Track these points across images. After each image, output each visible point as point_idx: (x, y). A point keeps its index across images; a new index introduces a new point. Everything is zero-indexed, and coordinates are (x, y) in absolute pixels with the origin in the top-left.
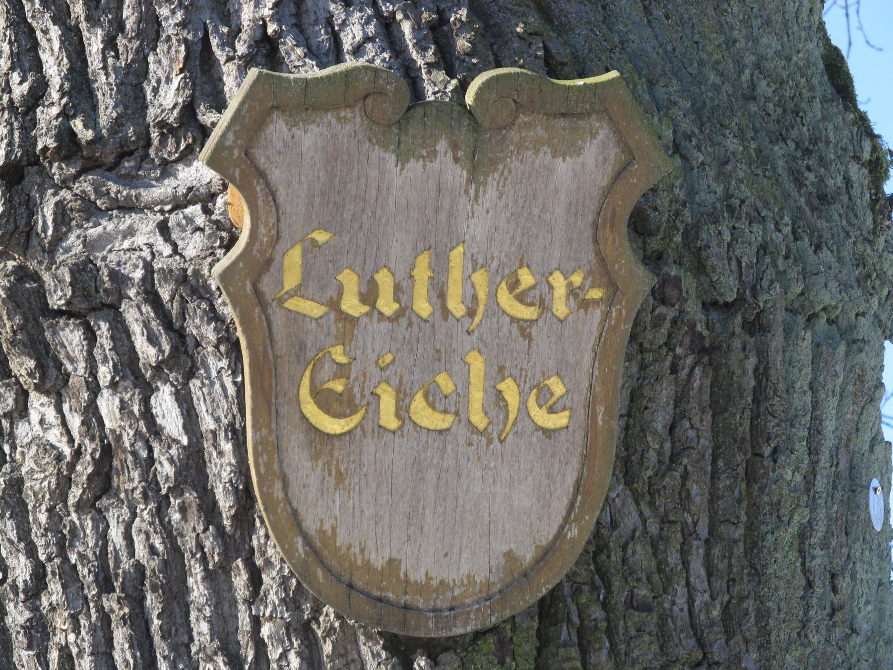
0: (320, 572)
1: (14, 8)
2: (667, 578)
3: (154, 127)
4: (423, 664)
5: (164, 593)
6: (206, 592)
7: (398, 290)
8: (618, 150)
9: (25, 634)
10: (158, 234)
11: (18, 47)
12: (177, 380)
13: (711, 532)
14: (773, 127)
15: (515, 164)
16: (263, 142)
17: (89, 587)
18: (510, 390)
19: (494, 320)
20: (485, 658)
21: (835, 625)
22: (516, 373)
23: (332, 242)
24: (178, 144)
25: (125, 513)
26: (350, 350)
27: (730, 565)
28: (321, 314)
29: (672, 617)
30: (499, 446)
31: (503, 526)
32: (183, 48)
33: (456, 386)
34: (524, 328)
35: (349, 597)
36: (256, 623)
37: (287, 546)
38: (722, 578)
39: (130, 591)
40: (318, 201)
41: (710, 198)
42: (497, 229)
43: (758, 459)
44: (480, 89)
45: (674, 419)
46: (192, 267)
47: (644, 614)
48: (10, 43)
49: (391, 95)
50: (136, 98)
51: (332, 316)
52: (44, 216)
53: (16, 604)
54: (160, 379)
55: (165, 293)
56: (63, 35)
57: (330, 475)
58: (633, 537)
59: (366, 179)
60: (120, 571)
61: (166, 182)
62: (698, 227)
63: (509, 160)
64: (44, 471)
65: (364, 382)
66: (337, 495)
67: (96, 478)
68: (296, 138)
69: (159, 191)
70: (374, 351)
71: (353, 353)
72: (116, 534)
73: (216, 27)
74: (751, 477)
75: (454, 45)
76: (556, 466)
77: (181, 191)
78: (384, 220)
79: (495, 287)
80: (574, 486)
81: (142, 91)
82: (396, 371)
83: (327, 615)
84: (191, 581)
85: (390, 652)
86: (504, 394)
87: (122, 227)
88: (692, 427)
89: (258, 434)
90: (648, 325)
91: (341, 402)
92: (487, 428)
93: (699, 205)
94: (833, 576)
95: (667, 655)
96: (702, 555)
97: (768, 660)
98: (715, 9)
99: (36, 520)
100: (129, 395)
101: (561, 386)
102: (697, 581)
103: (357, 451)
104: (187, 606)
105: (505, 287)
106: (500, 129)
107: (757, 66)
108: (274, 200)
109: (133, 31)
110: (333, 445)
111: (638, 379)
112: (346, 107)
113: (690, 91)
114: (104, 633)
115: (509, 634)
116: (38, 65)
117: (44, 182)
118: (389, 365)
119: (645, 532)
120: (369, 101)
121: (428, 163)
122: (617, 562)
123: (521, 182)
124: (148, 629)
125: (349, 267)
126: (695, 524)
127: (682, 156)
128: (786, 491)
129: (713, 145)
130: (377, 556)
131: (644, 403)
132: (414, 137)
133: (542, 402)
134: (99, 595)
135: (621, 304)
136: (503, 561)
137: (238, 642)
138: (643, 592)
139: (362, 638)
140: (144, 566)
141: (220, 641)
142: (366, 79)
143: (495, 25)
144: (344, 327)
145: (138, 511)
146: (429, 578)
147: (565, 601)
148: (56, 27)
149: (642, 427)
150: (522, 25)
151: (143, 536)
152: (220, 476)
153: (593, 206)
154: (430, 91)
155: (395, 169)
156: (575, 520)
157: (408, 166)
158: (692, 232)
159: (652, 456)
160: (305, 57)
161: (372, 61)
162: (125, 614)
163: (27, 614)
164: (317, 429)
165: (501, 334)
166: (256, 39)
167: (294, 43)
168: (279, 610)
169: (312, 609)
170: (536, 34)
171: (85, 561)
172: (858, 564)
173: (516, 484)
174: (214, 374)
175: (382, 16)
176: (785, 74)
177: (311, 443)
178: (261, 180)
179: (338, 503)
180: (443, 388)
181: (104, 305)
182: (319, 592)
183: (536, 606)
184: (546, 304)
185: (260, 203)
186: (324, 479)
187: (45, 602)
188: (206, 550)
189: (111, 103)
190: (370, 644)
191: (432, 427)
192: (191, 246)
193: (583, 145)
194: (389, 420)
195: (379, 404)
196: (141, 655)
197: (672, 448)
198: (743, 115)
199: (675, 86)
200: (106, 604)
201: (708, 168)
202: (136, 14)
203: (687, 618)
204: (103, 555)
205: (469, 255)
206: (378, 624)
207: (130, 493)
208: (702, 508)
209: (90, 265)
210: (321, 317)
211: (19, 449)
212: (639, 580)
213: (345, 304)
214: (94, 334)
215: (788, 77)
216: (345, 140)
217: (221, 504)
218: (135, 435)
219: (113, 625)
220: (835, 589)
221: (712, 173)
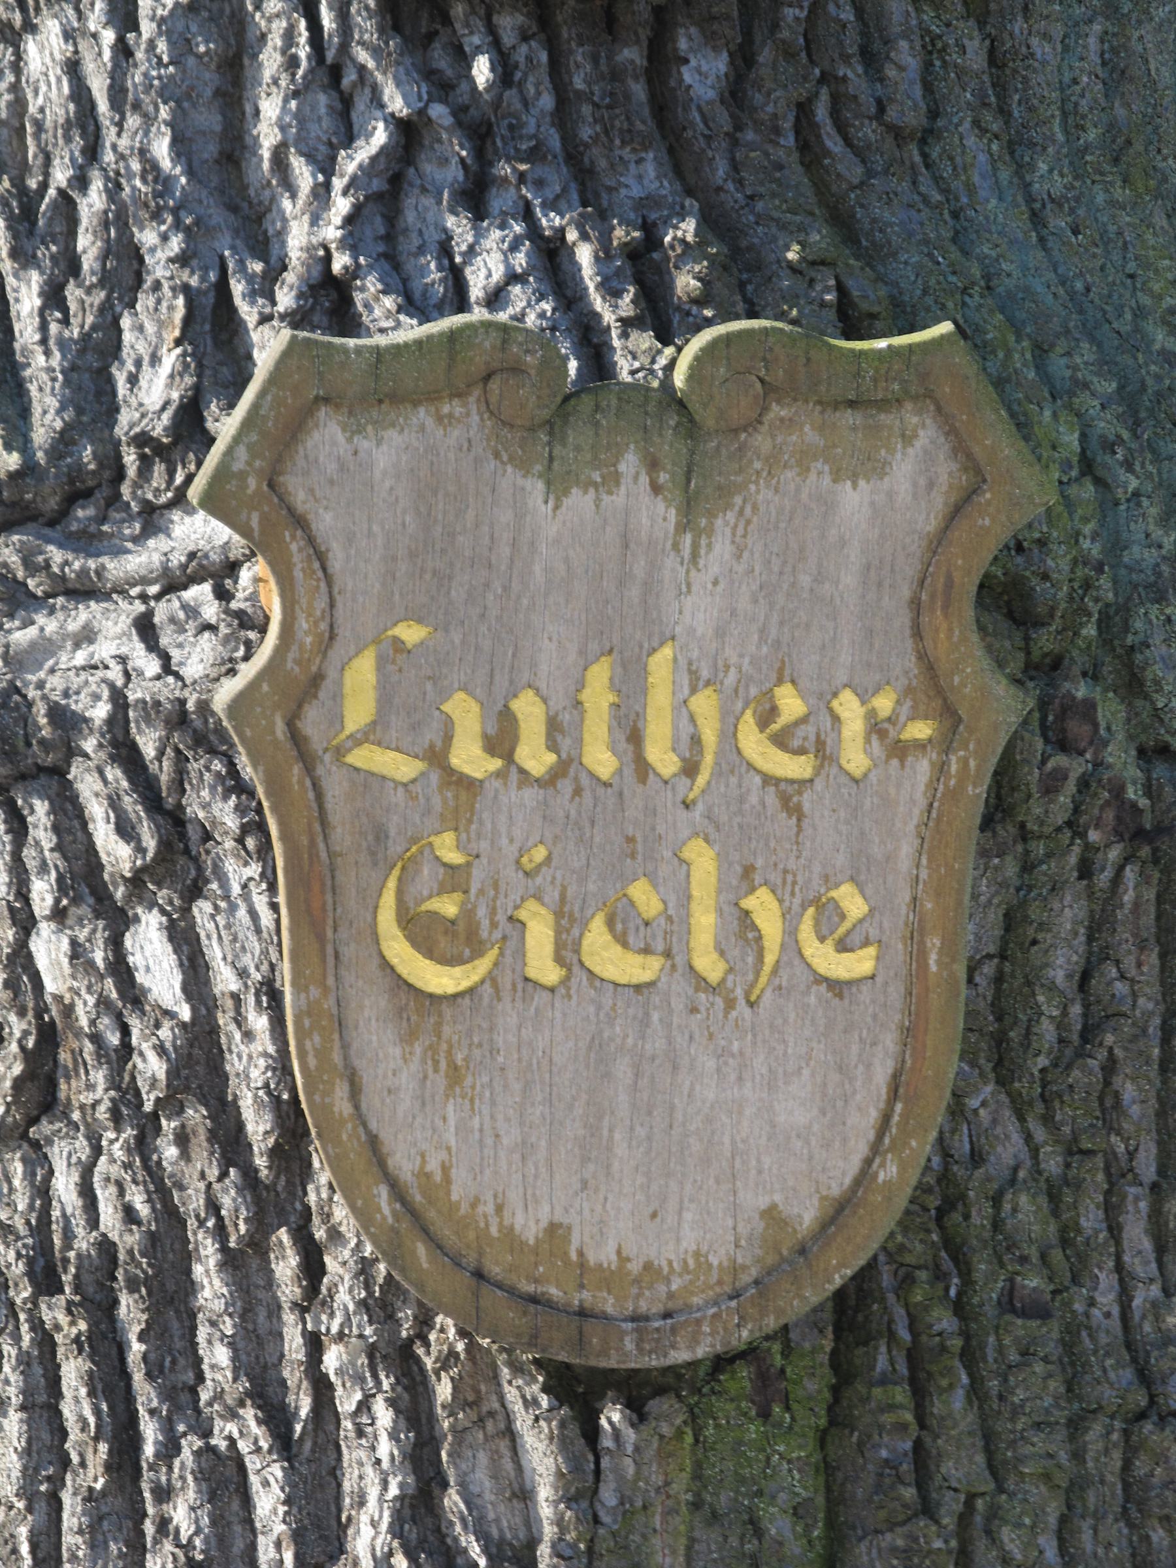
0: (421, 1250)
2: (1078, 1256)
3: (129, 445)
4: (616, 1417)
5: (149, 1294)
6: (225, 1291)
7: (554, 728)
8: (954, 466)
10: (135, 638)
12: (171, 903)
15: (764, 494)
16: (301, 462)
17: (16, 1285)
19: (733, 780)
20: (734, 1405)
22: (775, 877)
23: (431, 644)
24: (171, 473)
25: (84, 1153)
26: (469, 840)
28: (413, 775)
29: (1089, 1328)
30: (747, 1012)
31: (759, 1161)
32: (180, 301)
33: (664, 902)
35: (477, 1295)
36: (315, 1344)
37: (359, 1203)
39: (91, 1290)
40: (403, 567)
41: (1150, 557)
42: (734, 613)
44: (697, 358)
45: (1088, 961)
46: (195, 696)
47: (1034, 1323)
49: (533, 372)
50: (99, 394)
51: (435, 777)
55: (148, 743)
57: (436, 1071)
58: (1013, 1181)
59: (492, 526)
60: (72, 1254)
61: (151, 543)
62: (1128, 610)
63: (753, 487)
65: (494, 900)
66: (450, 1108)
67: (29, 1084)
68: (362, 454)
69: (138, 560)
70: (511, 841)
71: (473, 845)
72: (65, 1186)
73: (241, 263)
75: (670, 286)
76: (855, 1048)
77: (178, 559)
78: (525, 602)
79: (732, 720)
80: (889, 1085)
81: (110, 381)
82: (554, 878)
83: (442, 1330)
84: (198, 1270)
85: (557, 1398)
86: (754, 916)
87: (73, 626)
88: (1122, 977)
89: (303, 995)
90: (1034, 789)
91: (455, 935)
92: (723, 981)
93: (1130, 569)
95: (1080, 1399)
96: (1144, 1214)
98: (1169, 216)
100: (86, 931)
101: (860, 900)
102: (1137, 1261)
103: (485, 1025)
104: (193, 1316)
105: (751, 721)
106: (736, 431)
108: (324, 569)
109: (93, 273)
110: (440, 1015)
111: (1018, 890)
112: (452, 396)
113: (1116, 364)
114: (45, 1369)
115: (778, 1360)
118: (540, 865)
119: (1037, 1171)
120: (494, 385)
121: (604, 496)
122: (983, 1226)
123: (777, 528)
124: (123, 1360)
125: (464, 689)
126: (1131, 1155)
127: (1099, 482)
129: (1157, 459)
130: (527, 1220)
131: (1031, 932)
132: (578, 449)
133: (825, 931)
134: (34, 1300)
135: (966, 748)
136: (760, 1226)
137: (283, 1382)
138: (1033, 1282)
139: (505, 1372)
140: (114, 1244)
141: (250, 1380)
142: (487, 344)
143: (750, 248)
144: (456, 797)
145: (104, 1143)
146: (623, 1259)
147: (883, 1300)
149: (1026, 976)
150: (797, 247)
151: (113, 1190)
152: (248, 1076)
153: (909, 570)
154: (624, 367)
155: (543, 508)
157: (567, 502)
158: (1117, 619)
159: (1047, 1030)
160: (398, 312)
161: (520, 317)
162: (80, 1334)
164: (410, 986)
165: (747, 806)
166: (312, 282)
167: (380, 286)
169: (415, 1317)
170: (823, 263)
171: (11, 1237)
173: (780, 1083)
174: (236, 890)
175: (541, 237)
177: (400, 1011)
178: (299, 533)
180: (642, 908)
181: (41, 769)
182: (421, 1288)
183: (830, 1304)
184: (828, 753)
185: (298, 574)
186: (425, 1077)
188: (223, 1212)
189: (53, 403)
190: (520, 1382)
191: (623, 980)
192: (195, 658)
193: (889, 458)
194: (543, 968)
195: (523, 938)
196: (109, 1407)
197: (1085, 1015)
199: (1086, 353)
200: (47, 1316)
201: (1145, 502)
202: (99, 244)
203: (1119, 1331)
204: (42, 1228)
205: (683, 662)
207: (89, 1112)
208: (1144, 1124)
209: (16, 698)
210: (414, 781)
212: (1024, 1259)
213: (457, 757)
216: (451, 456)
217: (250, 1128)
218: (97, 1005)
219: (61, 1351)
221: (1153, 511)
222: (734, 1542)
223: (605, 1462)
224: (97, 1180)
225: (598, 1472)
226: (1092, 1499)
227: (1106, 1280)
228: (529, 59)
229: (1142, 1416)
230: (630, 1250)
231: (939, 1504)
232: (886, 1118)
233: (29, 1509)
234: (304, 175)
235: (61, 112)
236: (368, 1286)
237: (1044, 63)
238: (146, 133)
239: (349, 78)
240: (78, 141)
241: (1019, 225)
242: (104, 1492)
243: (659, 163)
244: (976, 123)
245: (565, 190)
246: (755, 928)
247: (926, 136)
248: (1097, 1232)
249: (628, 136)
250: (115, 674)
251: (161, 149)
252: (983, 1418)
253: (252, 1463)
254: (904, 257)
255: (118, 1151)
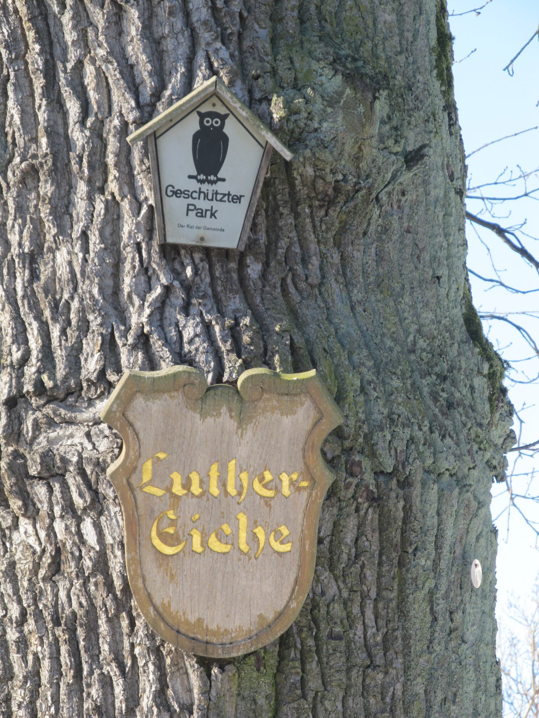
0: (162, 625)
1: (15, 310)
4: (216, 671)
5: (86, 628)
7: (201, 482)
8: (315, 412)
9: (16, 645)
11: (17, 330)
13: (378, 595)
14: (424, 367)
18: (260, 533)
19: (252, 497)
21: (451, 640)
24: (96, 390)
25: (68, 585)
27: (388, 613)
30: (255, 561)
32: (100, 338)
34: (267, 501)
36: (132, 646)
38: (383, 620)
39: (69, 625)
41: (380, 417)
43: (406, 554)
47: (337, 642)
48: (12, 329)
50: (76, 363)
51: (168, 495)
52: (27, 426)
53: (12, 628)
54: (85, 514)
56: (39, 326)
57: (167, 575)
61: (90, 409)
64: (26, 559)
72: (62, 595)
73: (118, 326)
74: (401, 564)
76: (285, 571)
84: (100, 622)
87: (67, 433)
88: (367, 540)
90: (342, 488)
93: (374, 421)
94: (451, 613)
97: (410, 662)
99: (22, 585)
101: (287, 530)
104: (98, 634)
106: (254, 401)
107: (419, 331)
108: (138, 438)
111: (337, 516)
115: (263, 654)
116: (26, 341)
117: (27, 407)
120: (186, 388)
125: (176, 471)
126: (369, 591)
128: (421, 571)
131: (341, 528)
132: (209, 406)
134: (53, 628)
137: (123, 656)
138: (338, 629)
141: (114, 654)
143: (266, 324)
146: (219, 628)
147: (294, 636)
148: (36, 322)
151: (76, 597)
153: (302, 440)
156: (294, 599)
157: (206, 420)
159: (345, 557)
163: (17, 635)
164: (160, 552)
168: (144, 640)
170: (286, 331)
172: (468, 604)
174: (113, 514)
176: (436, 333)
177: (157, 559)
179: (171, 590)
181: (57, 474)
185: (130, 439)
187: (26, 629)
189: (63, 366)
192: (102, 445)
197: (356, 551)
198: (406, 363)
204: (56, 606)
206: (192, 651)
211: (14, 546)
212: (335, 623)
214: (52, 488)
215: (438, 334)
217: (115, 583)
218: (73, 543)
219: (60, 643)
220: (452, 620)
222: (249, 705)
223: (213, 683)
224: (71, 594)
225: (211, 686)
226: (353, 691)
227: (360, 627)
228: (203, 267)
229: (368, 667)
230: (221, 625)
231: (307, 695)
232: (293, 590)
233: (51, 687)
234: (137, 301)
235: (66, 276)
236: (147, 630)
237: (357, 259)
238: (91, 286)
239: (150, 272)
240: (71, 286)
241: (347, 310)
242: (72, 684)
243: (240, 298)
244: (336, 280)
245: (212, 307)
246: (257, 537)
247: (321, 284)
248: (357, 614)
249: (231, 291)
250: (79, 448)
251: (95, 291)
252: (322, 669)
253: (114, 679)
254: (311, 326)
255: (78, 587)
